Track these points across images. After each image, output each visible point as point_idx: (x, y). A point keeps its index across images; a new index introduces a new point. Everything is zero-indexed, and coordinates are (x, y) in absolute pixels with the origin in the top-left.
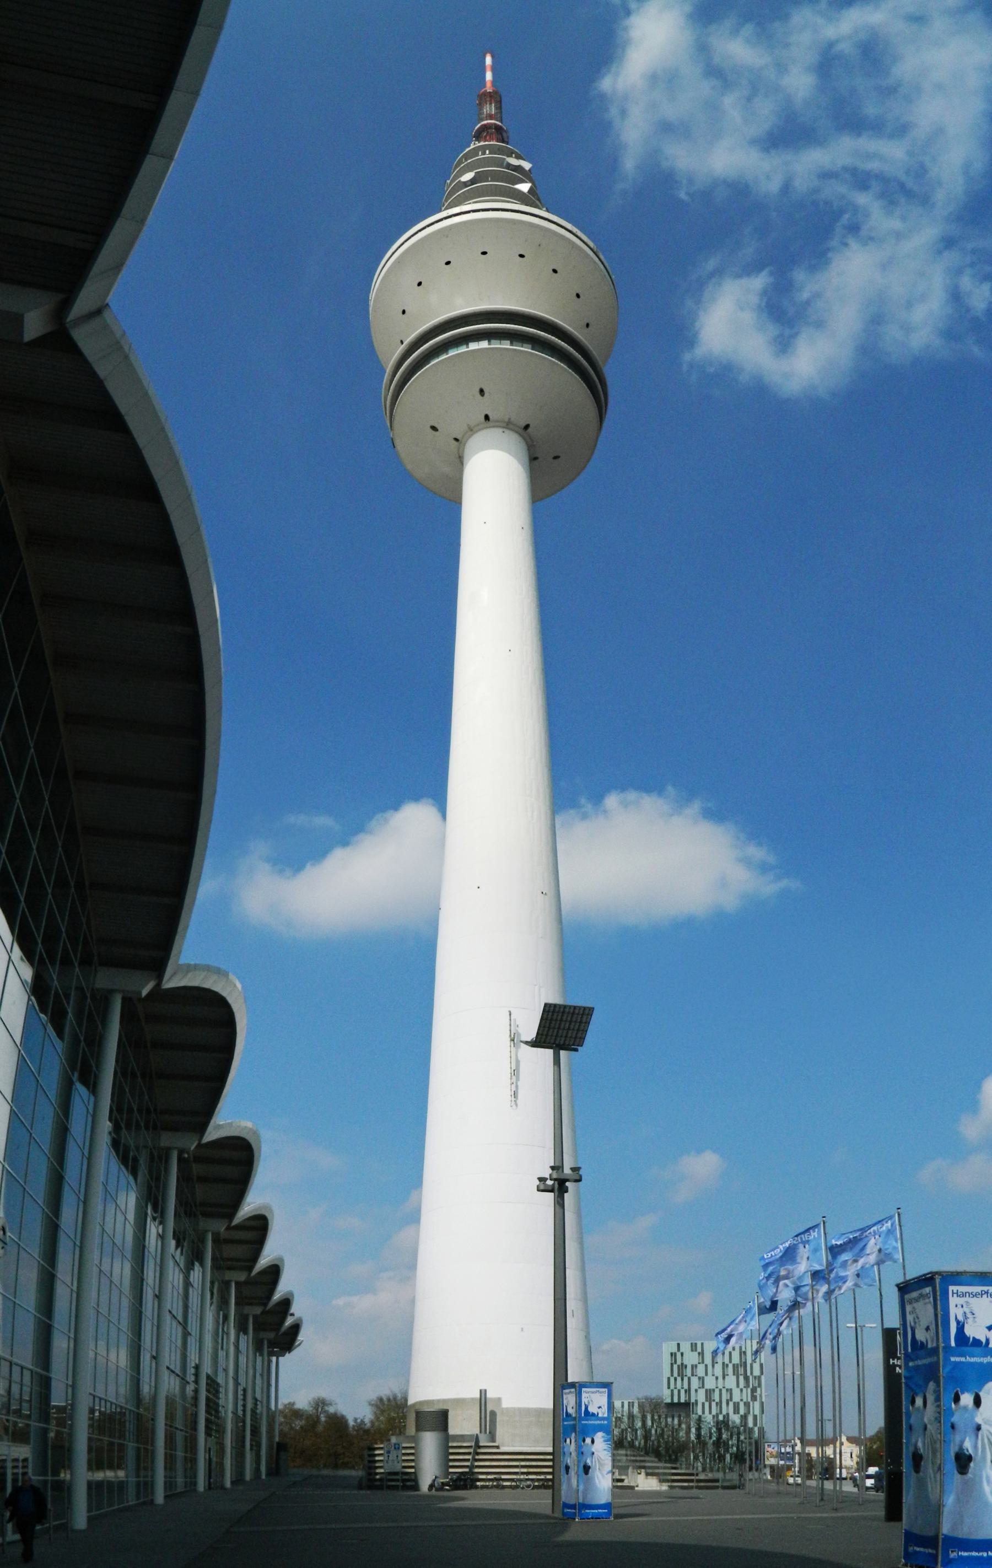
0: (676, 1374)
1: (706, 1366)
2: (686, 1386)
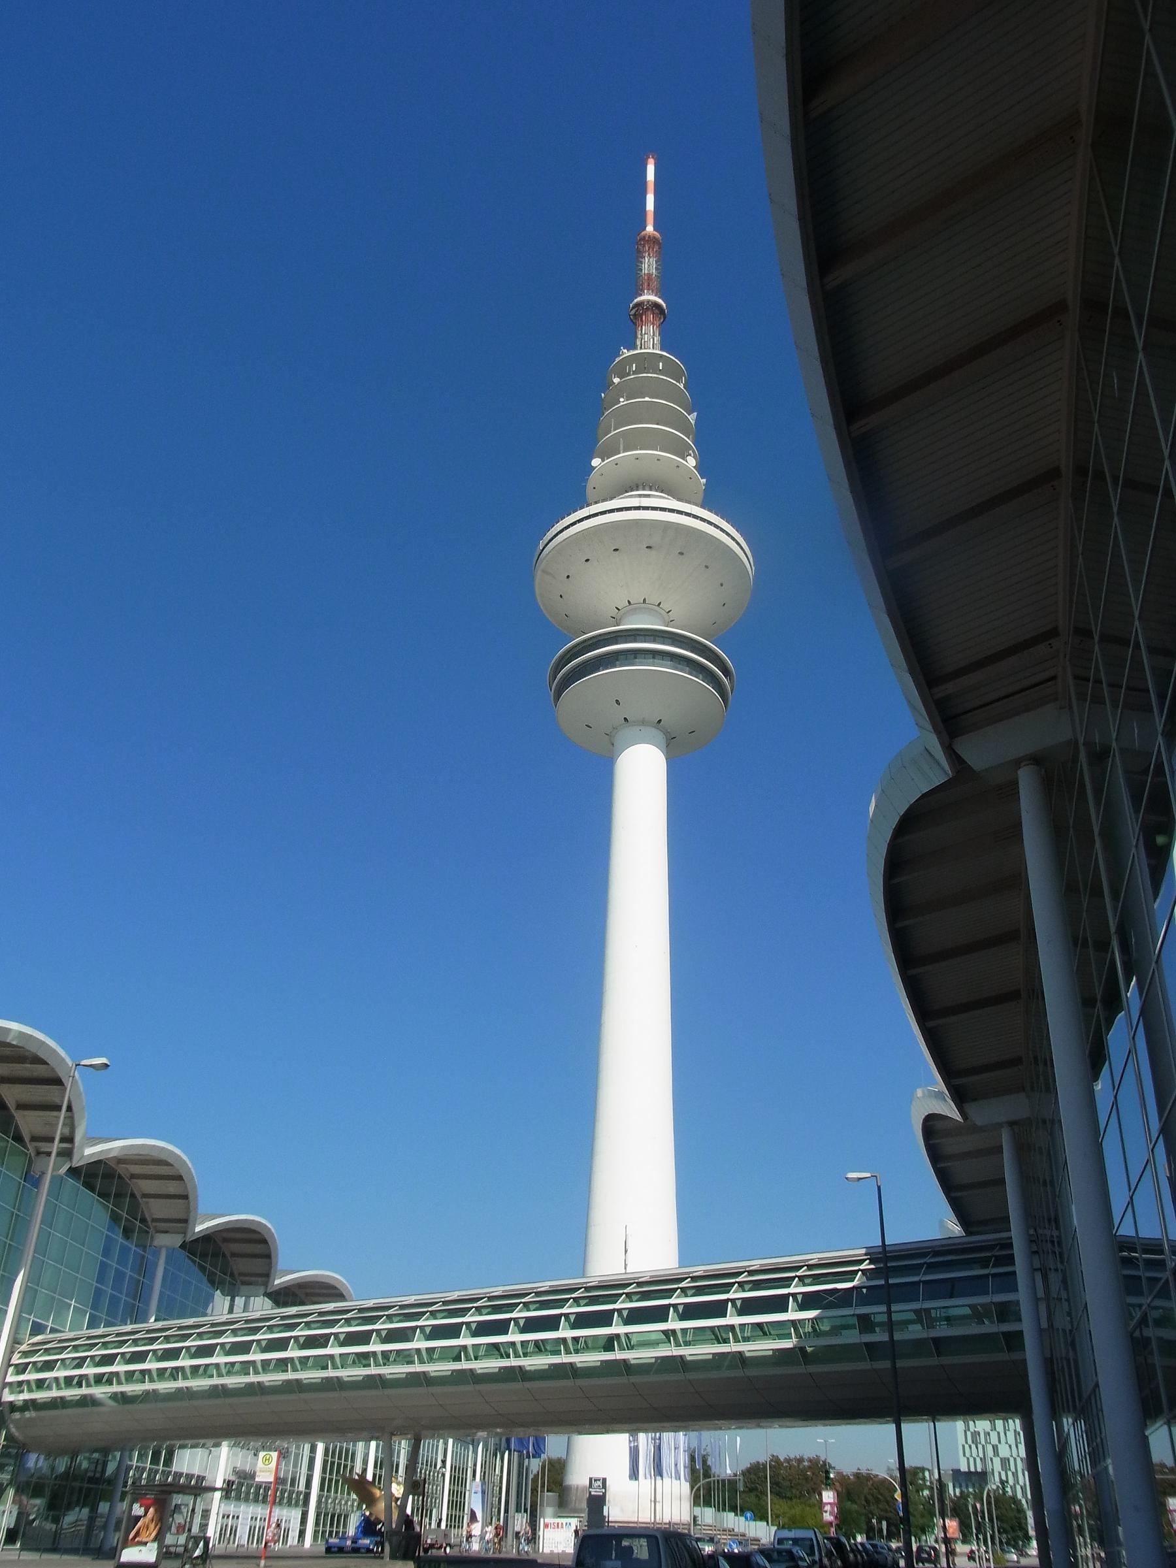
0: (970, 1441)
1: (999, 1433)
2: (981, 1455)
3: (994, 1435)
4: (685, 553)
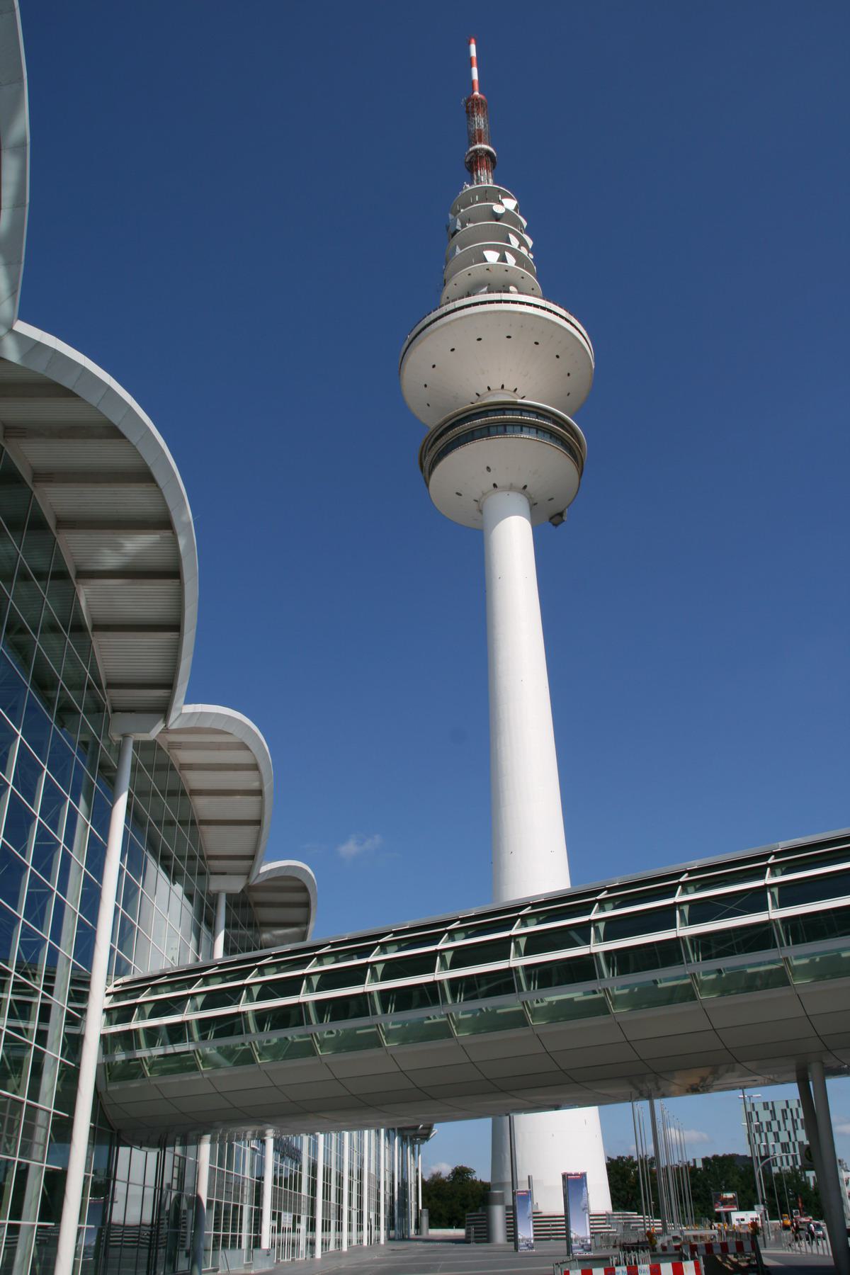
1: (779, 1122)
3: (774, 1124)
4: (540, 343)
